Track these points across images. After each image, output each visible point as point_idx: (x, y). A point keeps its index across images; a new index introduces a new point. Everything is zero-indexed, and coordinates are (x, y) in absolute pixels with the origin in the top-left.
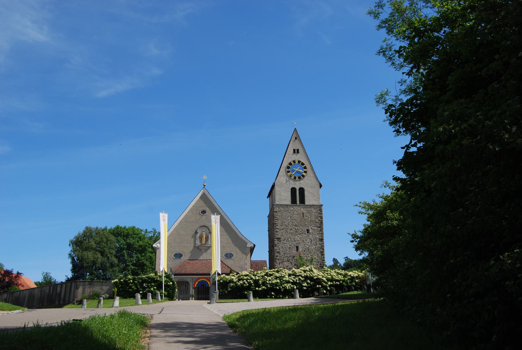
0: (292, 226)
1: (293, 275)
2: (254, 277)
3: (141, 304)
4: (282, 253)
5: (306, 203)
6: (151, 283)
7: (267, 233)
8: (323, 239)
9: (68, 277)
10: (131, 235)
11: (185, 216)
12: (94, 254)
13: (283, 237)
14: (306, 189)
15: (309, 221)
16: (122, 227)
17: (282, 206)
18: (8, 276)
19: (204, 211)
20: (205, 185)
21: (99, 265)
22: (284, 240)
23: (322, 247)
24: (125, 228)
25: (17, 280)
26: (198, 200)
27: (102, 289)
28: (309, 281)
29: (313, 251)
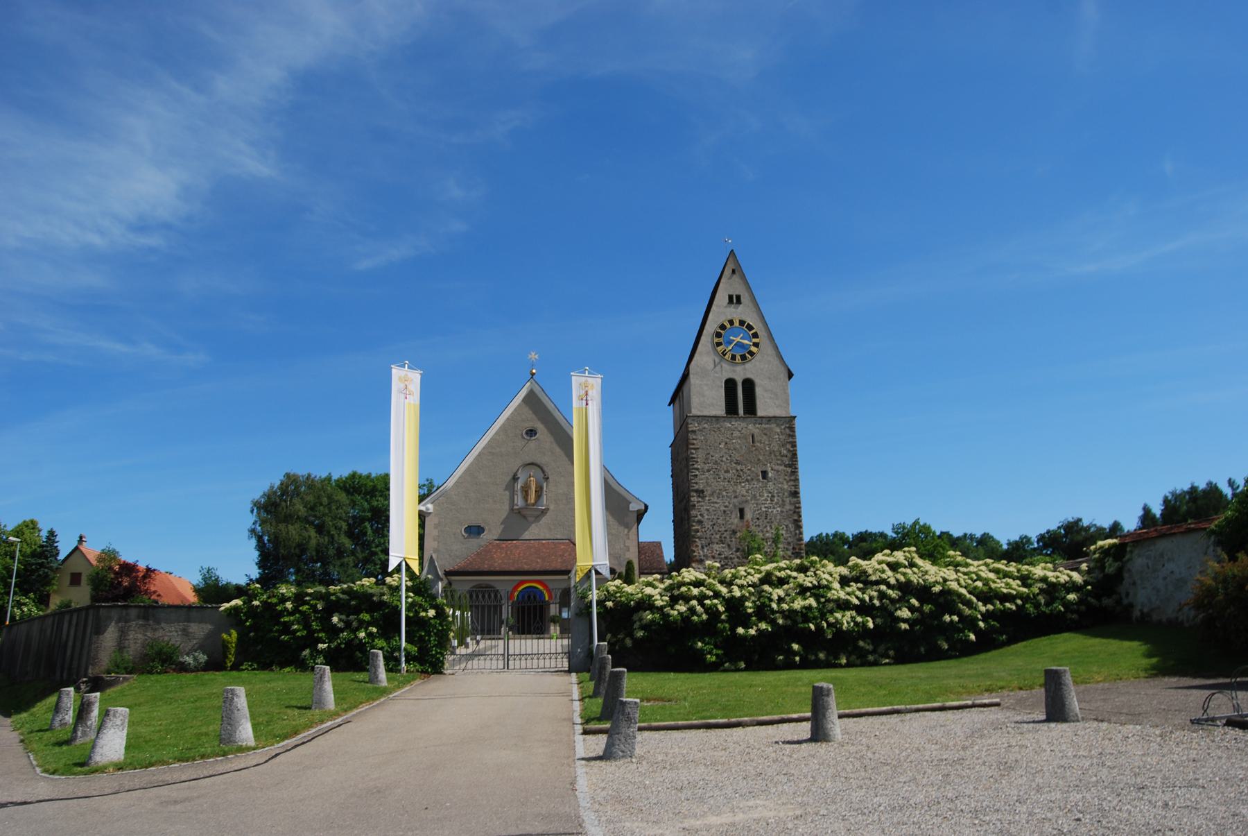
0: (728, 464)
1: (856, 580)
2: (724, 590)
3: (252, 743)
4: (708, 525)
5: (760, 413)
6: (357, 611)
7: (669, 482)
8: (798, 493)
9: (251, 577)
10: (381, 491)
11: (489, 441)
12: (301, 530)
13: (708, 488)
14: (757, 381)
15: (767, 453)
16: (363, 475)
17: (707, 418)
18: (127, 575)
19: (531, 430)
20: (534, 374)
21: (311, 552)
22: (712, 495)
23: (797, 510)
24: (369, 476)
25: (146, 583)
26: (519, 405)
27: (185, 632)
28: (914, 601)
29: (776, 519)
